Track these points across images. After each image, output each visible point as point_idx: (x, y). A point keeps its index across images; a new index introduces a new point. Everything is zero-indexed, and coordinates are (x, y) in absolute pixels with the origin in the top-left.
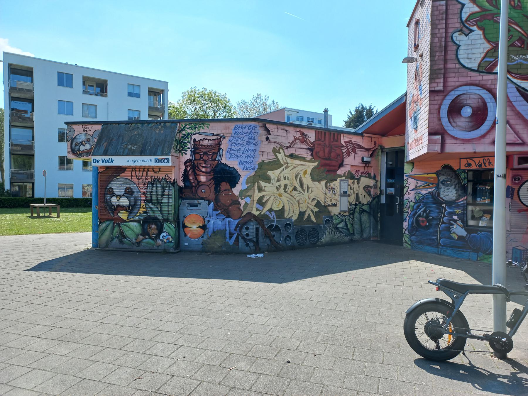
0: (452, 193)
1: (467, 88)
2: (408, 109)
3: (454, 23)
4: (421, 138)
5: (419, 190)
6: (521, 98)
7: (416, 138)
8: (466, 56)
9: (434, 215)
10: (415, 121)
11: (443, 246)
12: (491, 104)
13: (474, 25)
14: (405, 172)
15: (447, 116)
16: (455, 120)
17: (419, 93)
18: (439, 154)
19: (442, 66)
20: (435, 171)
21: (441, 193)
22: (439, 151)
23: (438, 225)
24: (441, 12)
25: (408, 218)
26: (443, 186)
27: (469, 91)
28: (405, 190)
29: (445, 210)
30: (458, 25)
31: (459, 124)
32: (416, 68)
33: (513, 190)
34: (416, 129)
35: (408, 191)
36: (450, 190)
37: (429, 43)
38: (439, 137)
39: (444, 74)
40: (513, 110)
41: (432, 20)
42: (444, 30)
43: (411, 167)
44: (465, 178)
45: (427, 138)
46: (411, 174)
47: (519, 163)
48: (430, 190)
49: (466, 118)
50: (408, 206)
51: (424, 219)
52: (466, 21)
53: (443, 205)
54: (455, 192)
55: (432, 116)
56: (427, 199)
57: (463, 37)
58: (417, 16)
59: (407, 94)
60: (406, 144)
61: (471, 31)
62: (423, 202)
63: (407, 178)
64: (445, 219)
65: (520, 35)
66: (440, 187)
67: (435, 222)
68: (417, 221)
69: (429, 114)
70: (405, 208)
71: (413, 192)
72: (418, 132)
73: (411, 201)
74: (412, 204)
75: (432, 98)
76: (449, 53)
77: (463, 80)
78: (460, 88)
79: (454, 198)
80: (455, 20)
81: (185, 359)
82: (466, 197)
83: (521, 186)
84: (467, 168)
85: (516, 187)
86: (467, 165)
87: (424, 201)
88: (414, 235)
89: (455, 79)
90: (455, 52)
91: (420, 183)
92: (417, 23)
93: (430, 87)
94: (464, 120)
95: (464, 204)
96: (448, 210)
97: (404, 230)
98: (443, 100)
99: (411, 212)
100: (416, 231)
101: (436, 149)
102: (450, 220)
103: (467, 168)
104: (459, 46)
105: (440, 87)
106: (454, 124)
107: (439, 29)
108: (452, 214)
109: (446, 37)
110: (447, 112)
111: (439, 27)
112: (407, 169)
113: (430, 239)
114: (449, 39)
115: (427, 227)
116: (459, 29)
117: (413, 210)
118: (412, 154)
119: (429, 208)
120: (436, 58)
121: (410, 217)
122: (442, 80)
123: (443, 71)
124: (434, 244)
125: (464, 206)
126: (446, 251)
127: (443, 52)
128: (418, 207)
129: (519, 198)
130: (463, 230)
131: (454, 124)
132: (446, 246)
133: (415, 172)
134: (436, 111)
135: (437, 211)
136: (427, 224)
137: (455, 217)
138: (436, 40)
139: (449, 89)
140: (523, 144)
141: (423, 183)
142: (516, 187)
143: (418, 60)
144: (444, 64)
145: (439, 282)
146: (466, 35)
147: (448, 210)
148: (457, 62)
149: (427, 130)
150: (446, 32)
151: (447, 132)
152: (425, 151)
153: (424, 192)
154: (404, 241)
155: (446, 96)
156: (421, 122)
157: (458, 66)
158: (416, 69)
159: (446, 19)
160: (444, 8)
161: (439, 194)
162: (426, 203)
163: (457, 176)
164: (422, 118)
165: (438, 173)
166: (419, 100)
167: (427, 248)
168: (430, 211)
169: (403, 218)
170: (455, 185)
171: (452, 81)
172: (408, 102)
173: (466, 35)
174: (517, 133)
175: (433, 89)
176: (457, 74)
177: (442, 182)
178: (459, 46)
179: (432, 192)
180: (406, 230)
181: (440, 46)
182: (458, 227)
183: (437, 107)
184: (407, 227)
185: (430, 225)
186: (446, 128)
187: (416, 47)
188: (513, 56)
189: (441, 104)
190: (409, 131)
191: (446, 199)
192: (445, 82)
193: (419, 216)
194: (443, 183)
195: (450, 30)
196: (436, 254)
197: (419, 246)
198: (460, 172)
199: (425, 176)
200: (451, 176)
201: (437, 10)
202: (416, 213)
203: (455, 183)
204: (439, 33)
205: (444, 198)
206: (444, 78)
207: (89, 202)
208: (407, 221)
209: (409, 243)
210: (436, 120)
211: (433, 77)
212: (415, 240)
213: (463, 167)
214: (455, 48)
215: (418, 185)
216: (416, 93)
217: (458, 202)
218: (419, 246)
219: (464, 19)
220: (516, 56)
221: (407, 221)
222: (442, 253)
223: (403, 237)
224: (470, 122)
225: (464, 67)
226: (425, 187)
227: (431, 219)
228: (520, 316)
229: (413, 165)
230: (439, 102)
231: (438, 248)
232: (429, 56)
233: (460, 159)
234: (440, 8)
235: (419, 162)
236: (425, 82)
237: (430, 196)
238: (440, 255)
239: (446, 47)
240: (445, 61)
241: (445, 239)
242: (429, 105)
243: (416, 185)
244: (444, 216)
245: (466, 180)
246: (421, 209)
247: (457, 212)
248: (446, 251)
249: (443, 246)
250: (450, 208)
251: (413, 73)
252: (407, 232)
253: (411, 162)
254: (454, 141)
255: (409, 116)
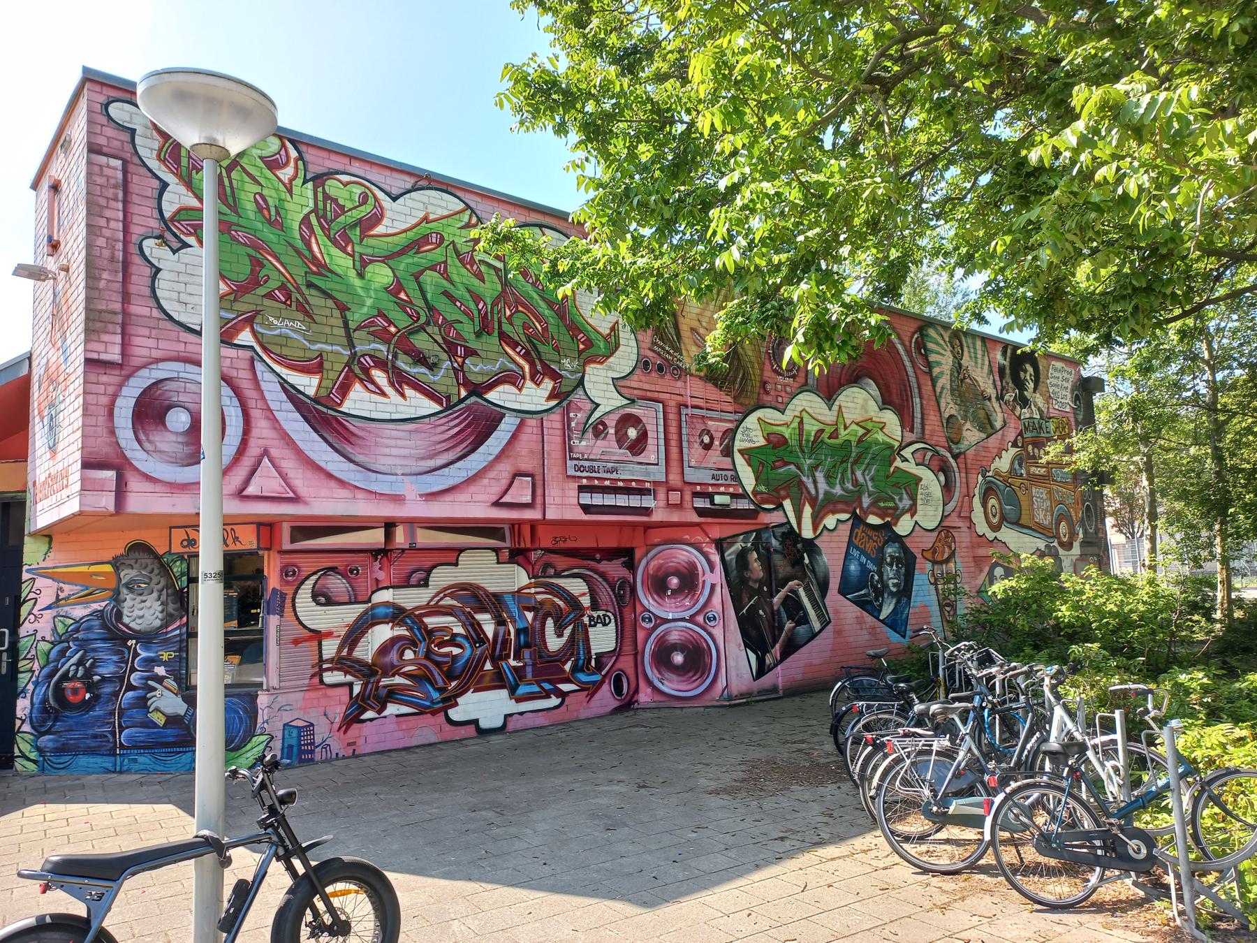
0: (152, 611)
1: (179, 366)
2: (36, 395)
3: (144, 220)
4: (64, 475)
5: (66, 609)
6: (290, 406)
7: (53, 471)
8: (175, 295)
9: (106, 670)
10: (51, 428)
11: (128, 748)
12: (232, 409)
13: (190, 234)
14: (26, 560)
15: (130, 425)
16: (151, 437)
17: (62, 359)
18: (111, 515)
19: (117, 306)
20: (109, 556)
21: (125, 612)
22: (111, 508)
23: (116, 694)
24: (113, 181)
25: (31, 687)
26: (131, 595)
27: (182, 375)
28: (24, 610)
29: (136, 655)
30: (154, 224)
31: (161, 446)
32: (55, 295)
33: (283, 596)
34: (53, 449)
35: (35, 611)
36: (148, 604)
37: (83, 244)
38: (110, 474)
39: (124, 326)
40: (275, 429)
41: (88, 193)
42: (120, 226)
43: (45, 547)
44: (182, 574)
45: (77, 476)
46: (43, 565)
47: (292, 542)
48: (96, 606)
49: (176, 433)
50: (33, 652)
51: (78, 685)
52: (172, 219)
53: (129, 643)
54: (160, 608)
55: (92, 421)
56: (89, 629)
57: (165, 253)
58: (55, 171)
59: (34, 357)
60: (30, 485)
61: (186, 245)
62: (77, 639)
63: (31, 576)
64: (135, 679)
65: (282, 279)
66: (122, 597)
67: (107, 689)
68: (59, 691)
69: (84, 415)
70: (25, 659)
71: (49, 614)
72: (59, 457)
73: (43, 639)
74: (44, 646)
75: (93, 378)
76: (134, 279)
77: (168, 347)
78: (162, 365)
79: (158, 623)
80: (148, 212)
81: (748, 912)
82: (185, 619)
83: (298, 588)
84: (187, 550)
85: (289, 591)
86: (185, 543)
87: (80, 635)
88: (48, 732)
89: (151, 343)
90: (148, 281)
91: (68, 589)
92: (55, 188)
93: (86, 350)
94: (173, 438)
95: (180, 635)
96: (143, 654)
97: (18, 723)
98: (121, 386)
99: (42, 668)
100: (56, 720)
101: (103, 504)
102: (148, 678)
103: (187, 550)
104: (158, 270)
105: (114, 354)
106: (147, 445)
107: (108, 220)
108: (150, 662)
109: (126, 243)
110: (130, 415)
111: (108, 213)
112: (33, 552)
113: (95, 736)
114: (134, 249)
115: (87, 706)
116: (157, 233)
117: (48, 663)
118: (43, 514)
119: (92, 654)
120: (102, 284)
121: (37, 684)
122: (118, 339)
123: (119, 318)
124: (105, 747)
125: (181, 641)
126: (135, 761)
127: (121, 274)
128: (62, 653)
129: (296, 615)
130: (179, 700)
131: (147, 445)
132: (136, 746)
133: (56, 559)
134: (103, 411)
135: (115, 658)
136: (88, 696)
137: (160, 671)
138: (101, 242)
139: (136, 362)
140: (296, 499)
141: (78, 588)
142: (289, 591)
143: (59, 279)
144: (123, 303)
145: (48, 866)
146: (174, 252)
147: (143, 654)
148: (152, 303)
149: (78, 455)
150: (126, 230)
151: (131, 464)
152: (73, 507)
153: (79, 612)
154: (17, 752)
155: (128, 377)
156: (65, 433)
157: (156, 313)
158: (54, 301)
159: (126, 202)
160: (120, 175)
161: (119, 615)
162: (83, 640)
163: (165, 569)
164: (67, 422)
165: (117, 563)
166: (61, 378)
167: (83, 760)
168: (95, 660)
169: (16, 688)
170: (160, 591)
171: (143, 346)
172: (35, 378)
173: (174, 252)
174: (284, 477)
175: (95, 356)
176: (154, 332)
177: (127, 586)
178: (158, 270)
179: (102, 611)
180: (23, 721)
181: (112, 259)
182: (166, 693)
183: (104, 400)
184: (27, 711)
185: (96, 698)
186: (129, 454)
187: (54, 246)
188: (271, 319)
189: (115, 396)
190: (38, 453)
191: (137, 628)
192: (125, 345)
193: (65, 677)
194: (130, 587)
195: (136, 230)
196: (109, 772)
197: (62, 760)
198: (170, 558)
199: (84, 569)
200: (150, 568)
201: (102, 175)
202: (56, 670)
203: (159, 587)
204: (107, 228)
205: (133, 625)
206: (123, 334)
207: (846, 51)
208: (29, 695)
209: (33, 756)
210: (102, 431)
211: (94, 324)
212: (50, 745)
213: (177, 548)
214: (148, 271)
215: (62, 595)
216: (54, 359)
217: (167, 633)
218: (62, 760)
219: (167, 215)
220: (277, 318)
221: (29, 695)
222: (125, 768)
223: (12, 742)
224: (187, 444)
225: (171, 318)
226: (83, 599)
227: (99, 681)
228: (248, 895)
229: (50, 543)
230: (111, 390)
231: (115, 755)
232: (82, 276)
233: (171, 528)
234: (107, 171)
235: (68, 533)
236: (74, 335)
237: (97, 623)
238: (121, 772)
239: (126, 265)
240: (126, 297)
241: (134, 730)
242: (85, 393)
243: (58, 596)
244: (133, 670)
245: (185, 578)
246: (71, 657)
247: (165, 657)
248: (135, 761)
249: (128, 748)
250: (147, 649)
251: (47, 308)
252: (27, 727)
253: (46, 533)
254: (148, 486)
255: (36, 412)
